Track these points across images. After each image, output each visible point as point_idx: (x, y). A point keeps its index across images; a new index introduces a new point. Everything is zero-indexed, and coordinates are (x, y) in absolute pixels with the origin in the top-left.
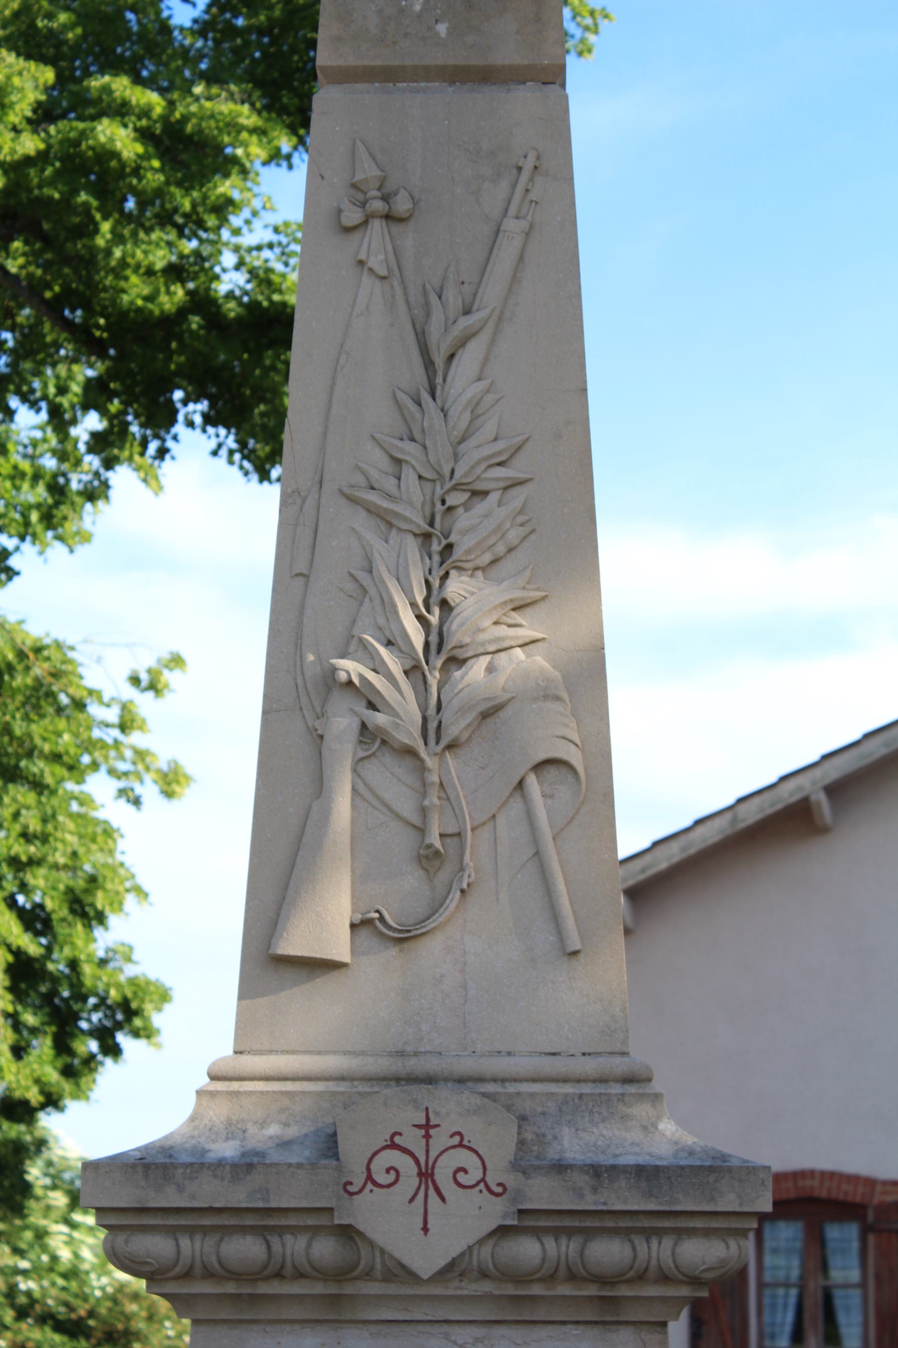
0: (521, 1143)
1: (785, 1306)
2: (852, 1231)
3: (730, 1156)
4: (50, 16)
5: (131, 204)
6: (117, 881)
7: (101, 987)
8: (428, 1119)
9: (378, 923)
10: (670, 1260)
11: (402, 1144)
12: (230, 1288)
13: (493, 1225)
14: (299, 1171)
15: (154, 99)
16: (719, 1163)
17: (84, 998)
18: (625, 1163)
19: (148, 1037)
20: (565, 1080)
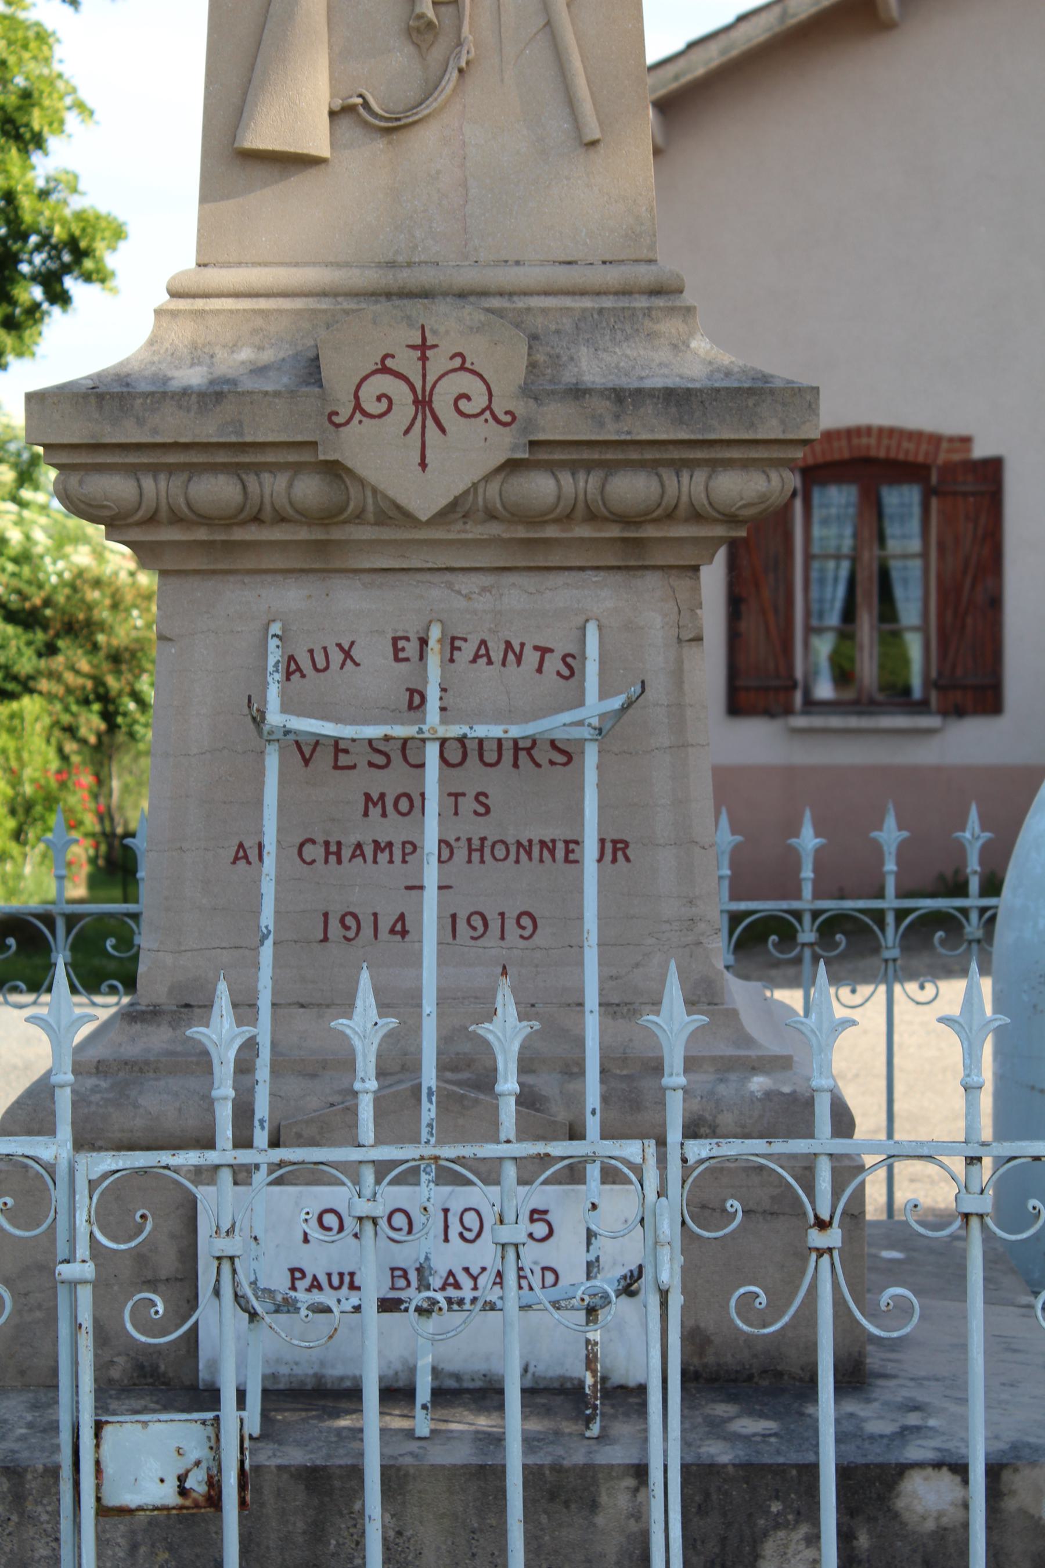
0: (532, 365)
1: (836, 580)
3: (772, 376)
6: (55, 96)
7: (43, 223)
8: (424, 339)
9: (361, 110)
10: (703, 496)
11: (395, 368)
12: (201, 534)
13: (501, 459)
14: (277, 401)
16: (760, 384)
17: (25, 237)
18: (653, 386)
19: (103, 281)
20: (583, 293)
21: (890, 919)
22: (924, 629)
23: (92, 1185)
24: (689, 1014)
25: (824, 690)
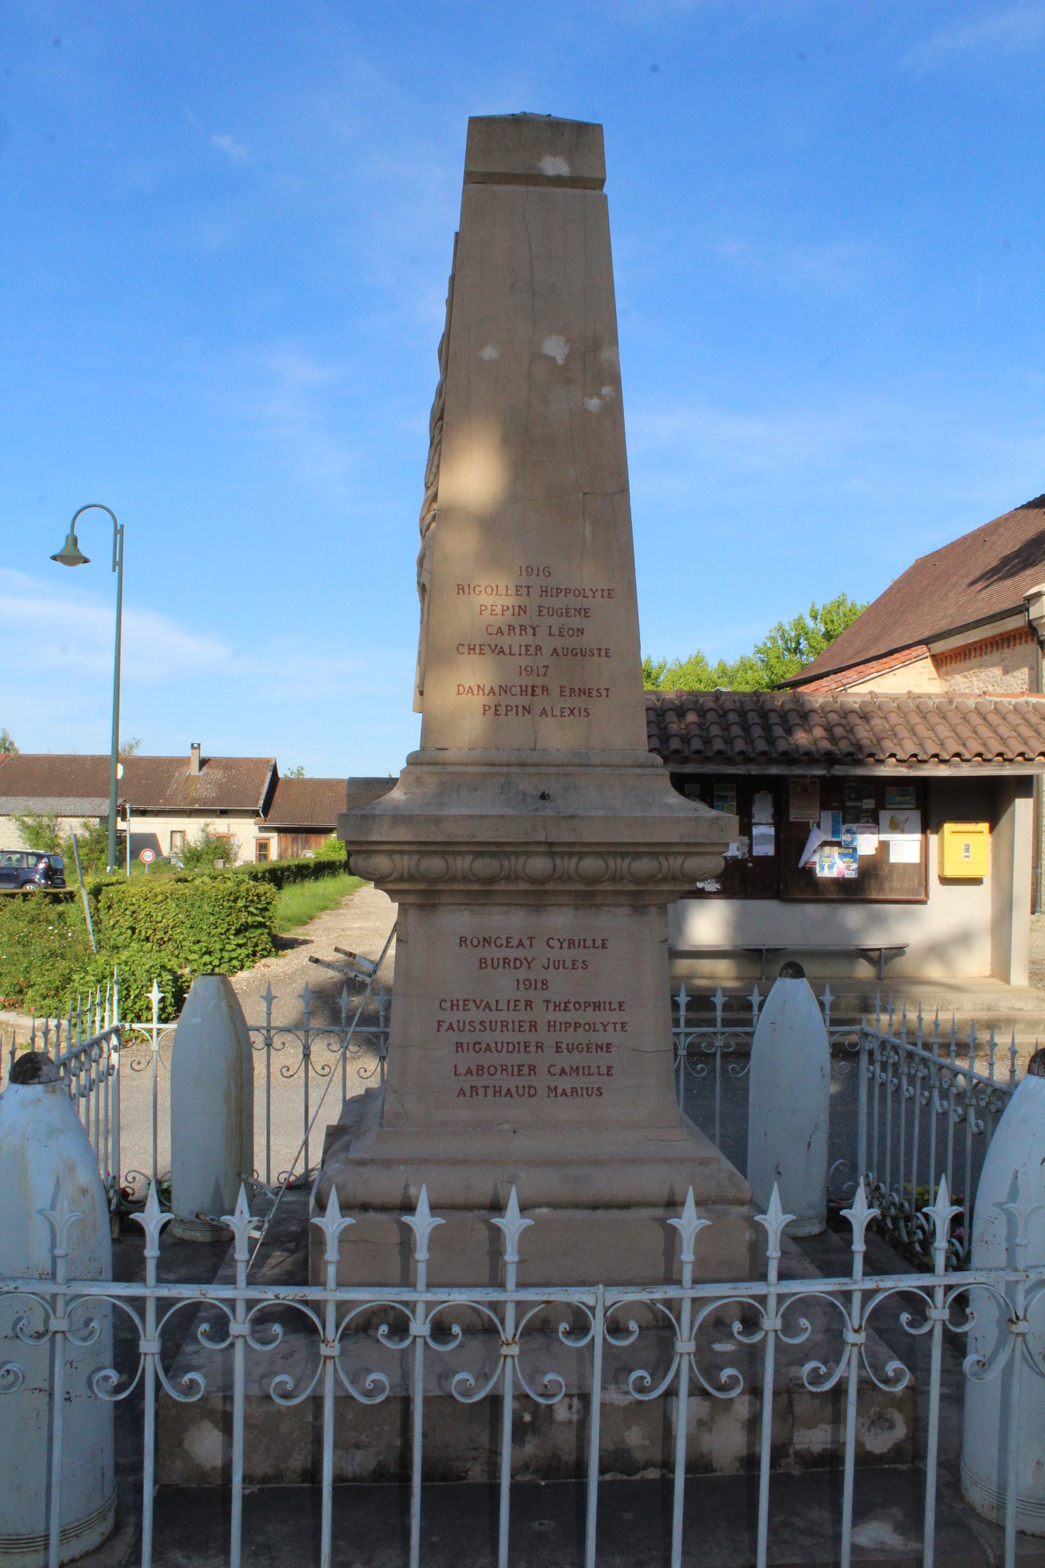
24: (343, 1216)
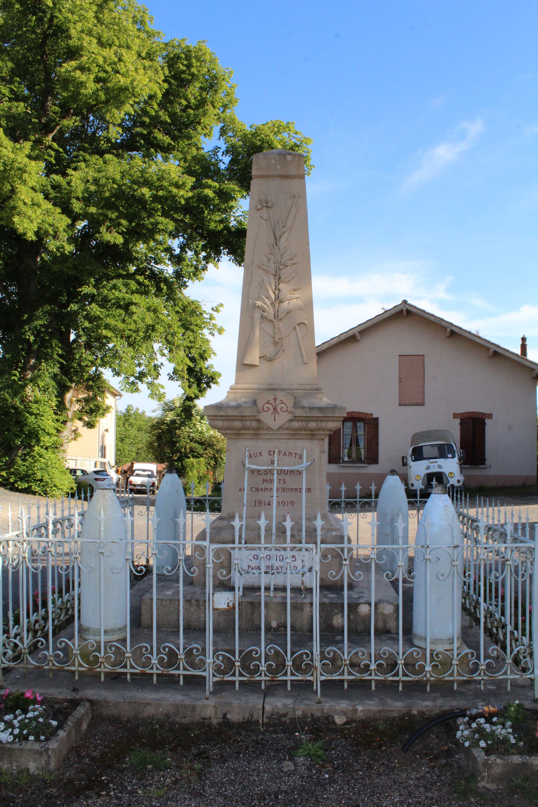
0: (295, 402)
2: (362, 424)
4: (195, 167)
5: (212, 207)
12: (235, 432)
15: (216, 184)
21: (400, 673)
22: (364, 448)
23: (213, 550)
25: (346, 459)
